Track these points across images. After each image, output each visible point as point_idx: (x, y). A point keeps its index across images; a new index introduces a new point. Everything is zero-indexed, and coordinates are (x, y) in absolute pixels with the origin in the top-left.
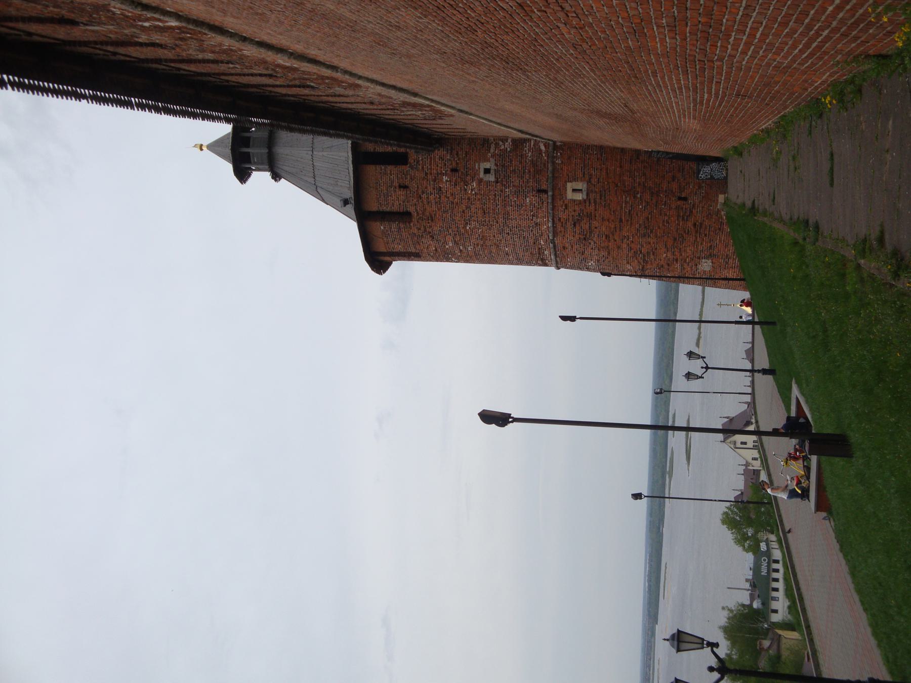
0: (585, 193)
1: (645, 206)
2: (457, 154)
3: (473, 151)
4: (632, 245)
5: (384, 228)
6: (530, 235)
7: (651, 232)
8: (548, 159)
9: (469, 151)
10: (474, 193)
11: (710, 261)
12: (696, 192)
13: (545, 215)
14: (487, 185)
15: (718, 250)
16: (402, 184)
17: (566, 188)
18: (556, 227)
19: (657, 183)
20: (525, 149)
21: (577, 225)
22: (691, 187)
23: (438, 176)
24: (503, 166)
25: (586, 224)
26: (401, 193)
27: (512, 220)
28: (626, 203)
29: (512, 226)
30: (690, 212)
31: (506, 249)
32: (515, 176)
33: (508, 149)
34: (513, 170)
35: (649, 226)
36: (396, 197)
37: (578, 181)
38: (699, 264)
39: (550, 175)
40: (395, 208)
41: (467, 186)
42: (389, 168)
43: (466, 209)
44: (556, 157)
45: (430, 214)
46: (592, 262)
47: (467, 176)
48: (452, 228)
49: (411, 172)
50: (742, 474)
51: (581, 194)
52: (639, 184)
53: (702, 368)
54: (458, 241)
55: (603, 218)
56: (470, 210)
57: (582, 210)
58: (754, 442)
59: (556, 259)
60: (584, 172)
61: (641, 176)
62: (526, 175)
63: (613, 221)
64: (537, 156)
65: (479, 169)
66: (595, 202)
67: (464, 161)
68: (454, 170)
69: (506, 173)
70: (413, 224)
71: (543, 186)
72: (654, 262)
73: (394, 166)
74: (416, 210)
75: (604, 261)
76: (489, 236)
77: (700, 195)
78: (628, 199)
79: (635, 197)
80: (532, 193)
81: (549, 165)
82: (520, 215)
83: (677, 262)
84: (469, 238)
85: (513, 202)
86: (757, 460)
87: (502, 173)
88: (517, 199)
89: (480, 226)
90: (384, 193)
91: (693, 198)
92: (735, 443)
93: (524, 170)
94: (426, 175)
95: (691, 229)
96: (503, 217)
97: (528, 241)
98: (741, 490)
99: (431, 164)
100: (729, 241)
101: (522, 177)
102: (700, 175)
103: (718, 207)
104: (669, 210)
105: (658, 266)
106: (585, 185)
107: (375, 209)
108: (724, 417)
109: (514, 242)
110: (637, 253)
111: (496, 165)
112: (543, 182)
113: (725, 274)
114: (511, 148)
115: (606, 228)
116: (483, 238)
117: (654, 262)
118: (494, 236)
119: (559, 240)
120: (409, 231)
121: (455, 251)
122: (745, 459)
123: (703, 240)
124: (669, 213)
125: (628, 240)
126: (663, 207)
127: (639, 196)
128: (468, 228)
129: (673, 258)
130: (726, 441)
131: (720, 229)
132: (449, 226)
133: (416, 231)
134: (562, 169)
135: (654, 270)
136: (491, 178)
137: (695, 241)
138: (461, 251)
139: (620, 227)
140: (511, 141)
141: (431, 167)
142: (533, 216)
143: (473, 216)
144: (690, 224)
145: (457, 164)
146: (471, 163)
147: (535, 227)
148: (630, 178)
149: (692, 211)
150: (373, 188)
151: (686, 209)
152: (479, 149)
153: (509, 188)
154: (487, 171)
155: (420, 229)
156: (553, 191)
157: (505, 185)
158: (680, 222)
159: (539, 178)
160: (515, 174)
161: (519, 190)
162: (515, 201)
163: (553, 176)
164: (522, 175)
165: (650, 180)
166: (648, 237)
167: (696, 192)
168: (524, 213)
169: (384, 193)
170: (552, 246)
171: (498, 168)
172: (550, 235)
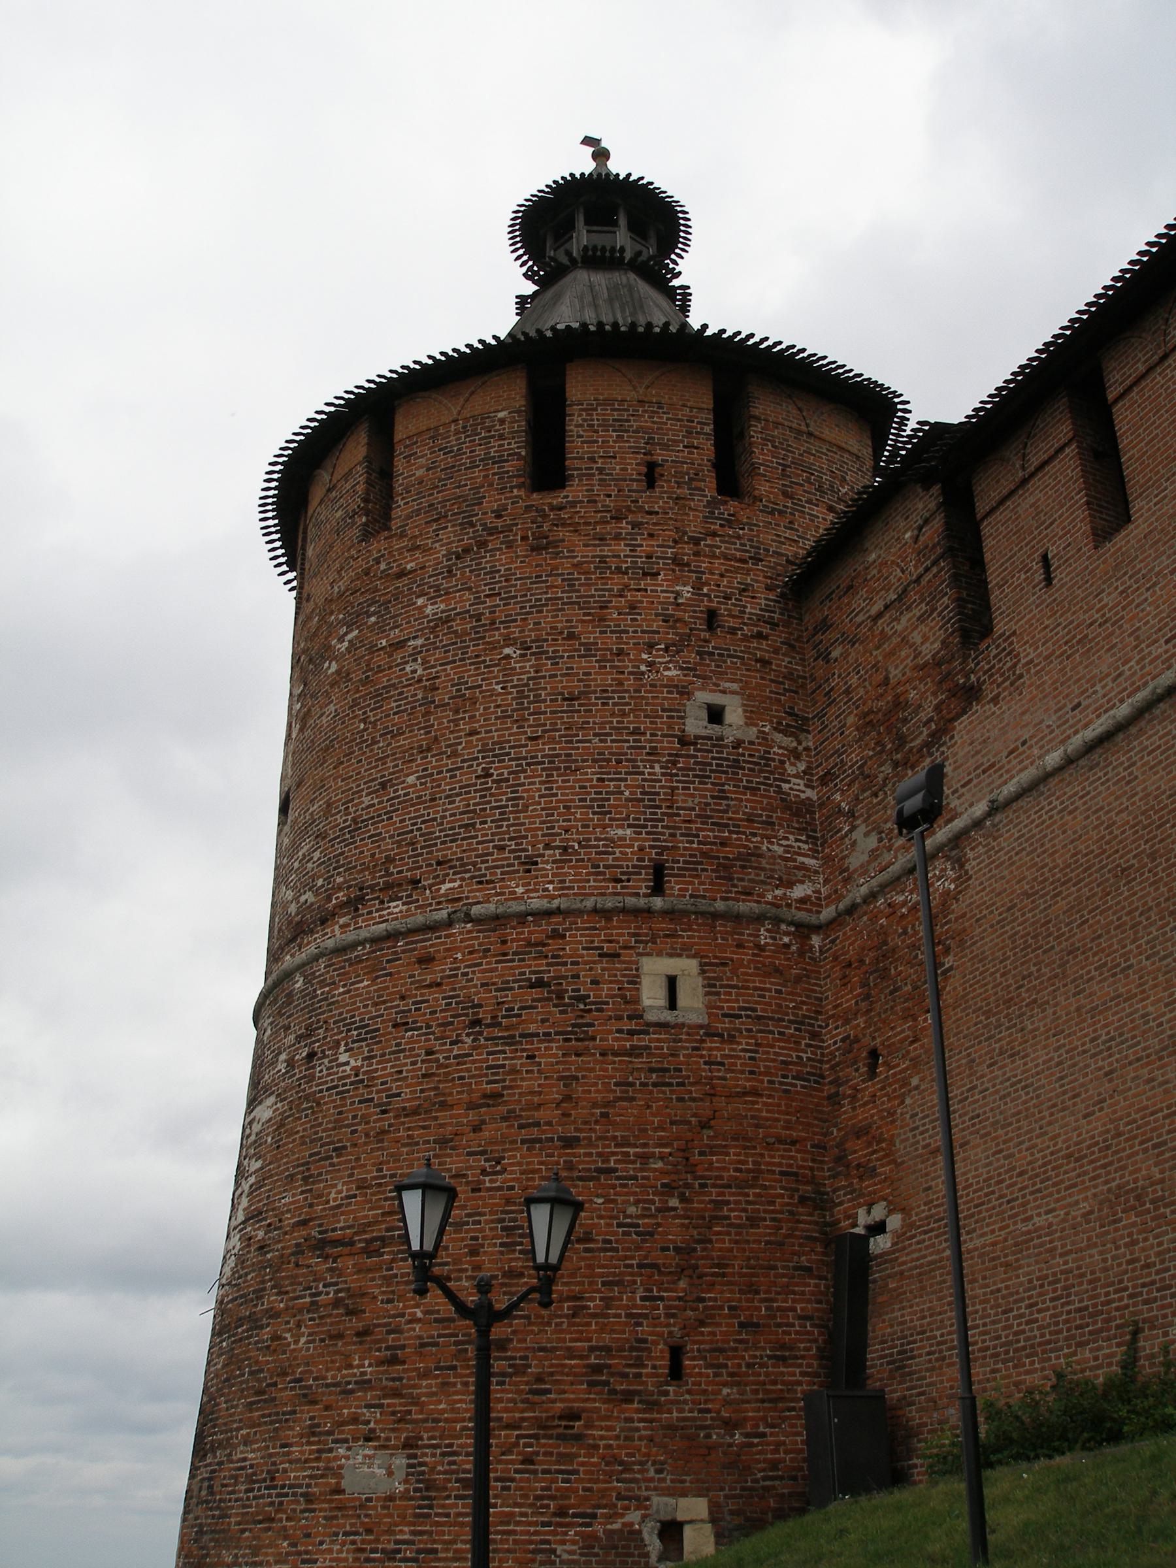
0: (667, 1016)
1: (638, 1226)
2: (760, 636)
3: (771, 681)
5: (502, 421)
8: (767, 903)
9: (771, 670)
10: (643, 668)
12: (708, 1411)
14: (671, 711)
16: (658, 470)
17: (680, 956)
18: (523, 923)
19: (726, 1266)
20: (791, 837)
21: (535, 993)
22: (725, 1391)
26: (633, 466)
28: (645, 1158)
30: (623, 1392)
32: (705, 797)
33: (785, 786)
34: (724, 791)
41: (666, 650)
42: (709, 446)
47: (698, 653)
52: (718, 1205)
55: (576, 1078)
57: (600, 1006)
59: (362, 943)
60: (740, 1016)
61: (745, 1210)
62: (712, 831)
64: (773, 870)
65: (724, 692)
66: (634, 1052)
68: (711, 617)
69: (711, 771)
71: (677, 883)
73: (712, 457)
74: (573, 504)
79: (668, 1189)
80: (651, 847)
82: (567, 808)
84: (455, 662)
87: (713, 758)
93: (727, 825)
96: (559, 755)
99: (726, 557)
101: (703, 818)
103: (656, 1500)
106: (695, 1018)
111: (738, 744)
112: (692, 883)
114: (789, 794)
116: (463, 702)
118: (473, 733)
125: (484, 1172)
131: (561, 1512)
134: (740, 945)
136: (696, 724)
139: (539, 1141)
140: (808, 799)
141: (719, 558)
142: (565, 849)
144: (576, 1395)
145: (733, 631)
146: (738, 668)
151: (639, 1375)
152: (780, 700)
153: (663, 774)
157: (674, 763)
159: (706, 870)
160: (713, 797)
161: (660, 807)
162: (622, 793)
163: (715, 916)
164: (711, 817)
165: (736, 1242)
167: (708, 1411)
172: (491, 907)
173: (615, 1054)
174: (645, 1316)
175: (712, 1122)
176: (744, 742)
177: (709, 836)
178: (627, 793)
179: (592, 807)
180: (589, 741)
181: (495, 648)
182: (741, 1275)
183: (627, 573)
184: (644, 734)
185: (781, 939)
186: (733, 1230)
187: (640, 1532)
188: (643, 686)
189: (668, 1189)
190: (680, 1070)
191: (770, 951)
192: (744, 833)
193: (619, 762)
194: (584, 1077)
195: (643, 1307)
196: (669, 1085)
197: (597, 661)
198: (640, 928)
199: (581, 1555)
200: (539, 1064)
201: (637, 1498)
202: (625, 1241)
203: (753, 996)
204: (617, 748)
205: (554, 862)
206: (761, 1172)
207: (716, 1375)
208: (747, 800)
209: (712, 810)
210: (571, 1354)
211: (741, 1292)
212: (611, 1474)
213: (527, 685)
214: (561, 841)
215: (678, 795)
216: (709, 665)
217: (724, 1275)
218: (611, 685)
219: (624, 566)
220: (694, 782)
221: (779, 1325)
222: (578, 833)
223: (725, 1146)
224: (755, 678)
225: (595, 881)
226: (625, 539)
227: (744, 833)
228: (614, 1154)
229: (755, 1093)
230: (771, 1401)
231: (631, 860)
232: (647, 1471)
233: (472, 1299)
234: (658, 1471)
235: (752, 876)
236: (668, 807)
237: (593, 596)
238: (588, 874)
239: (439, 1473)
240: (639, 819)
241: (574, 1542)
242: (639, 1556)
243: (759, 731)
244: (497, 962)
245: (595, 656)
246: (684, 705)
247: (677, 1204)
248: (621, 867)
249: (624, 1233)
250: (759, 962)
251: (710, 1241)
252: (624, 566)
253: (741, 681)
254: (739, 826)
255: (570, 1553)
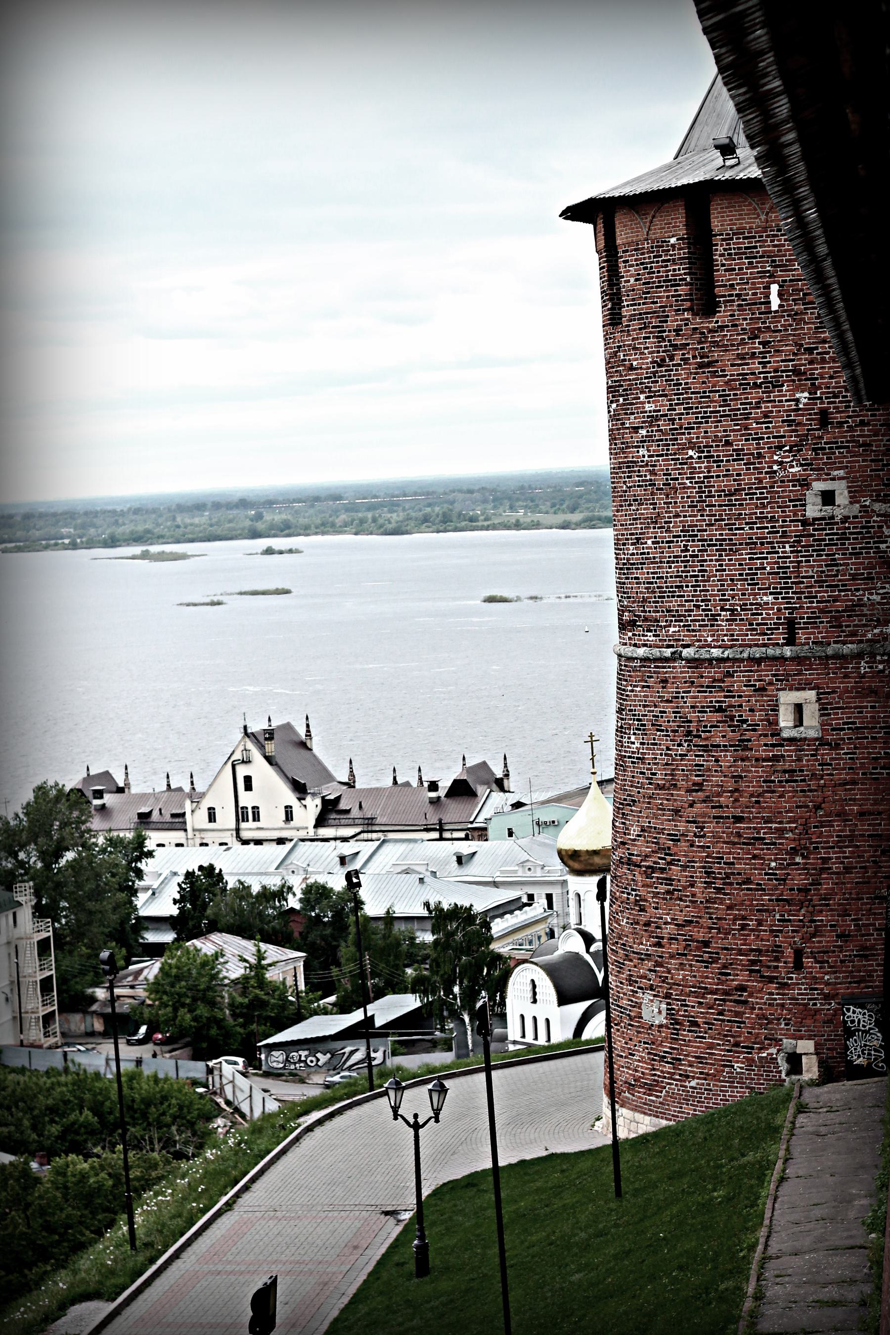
0: (794, 733)
1: (776, 874)
2: (862, 423)
3: (872, 461)
4: (683, 845)
5: (673, 246)
6: (686, 601)
7: (719, 890)
8: (868, 641)
9: (872, 451)
10: (775, 468)
11: (665, 1021)
12: (816, 989)
13: (737, 640)
15: (689, 1041)
17: (804, 689)
19: (829, 899)
21: (718, 716)
22: (827, 977)
23: (806, 380)
24: (843, 537)
25: (724, 736)
27: (717, 560)
28: (781, 831)
29: (706, 561)
31: (649, 542)
34: (835, 560)
35: (731, 884)
36: (748, 279)
37: (822, 715)
38: (655, 996)
39: (830, 651)
40: (721, 276)
41: (790, 451)
43: (734, 450)
44: (872, 661)
45: (717, 361)
46: (637, 745)
47: (814, 450)
48: (688, 414)
49: (812, 313)
50: (169, 785)
51: (791, 724)
52: (825, 860)
53: (416, 1116)
54: (659, 426)
55: (741, 777)
56: (734, 460)
58: (253, 808)
60: (844, 729)
61: (843, 863)
62: (827, 592)
63: (736, 800)
65: (833, 479)
66: (776, 758)
67: (847, 442)
68: (824, 418)
69: (826, 545)
70: (687, 319)
72: (649, 892)
74: (722, 328)
75: (642, 773)
76: (676, 503)
77: (809, 999)
78: (790, 835)
79: (794, 852)
80: (786, 608)
81: (855, 646)
83: (655, 945)
84: (667, 455)
85: (762, 564)
86: (210, 821)
87: (827, 535)
88: (769, 573)
89: (696, 483)
90: (756, 247)
91: (803, 984)
92: (246, 762)
93: (837, 586)
94: (805, 349)
95: (733, 980)
96: (725, 540)
97: (673, 597)
98: (127, 785)
100: (714, 1065)
102: (852, 1008)
103: (785, 1041)
104: (772, 931)
105: (641, 900)
106: (812, 734)
107: (716, 224)
108: (308, 726)
109: (668, 562)
110: (666, 854)
111: (845, 519)
112: (814, 633)
113: (639, 1051)
115: (718, 786)
116: (670, 489)
117: (649, 892)
118: (677, 516)
119: (682, 672)
120: (671, 306)
121: (633, 414)
122: (208, 790)
123: (709, 1008)
124: (765, 931)
125: (695, 836)
126: (777, 917)
127: (798, 859)
128: (691, 453)
129: (663, 938)
130: (247, 739)
131: (737, 1044)
132: (691, 408)
133: (672, 324)
134: (846, 676)
135: (633, 890)
137: (706, 988)
138: (636, 429)
139: (722, 817)
142: (732, 611)
143: (718, 466)
144: (742, 978)
145: (841, 424)
146: (845, 457)
147: (707, 615)
148: (837, 836)
149: (772, 982)
150: (767, 221)
151: (777, 967)
153: (792, 552)
154: (828, 498)
155: (678, 335)
156: (794, 659)
157: (799, 542)
158: (746, 955)
159: (823, 622)
160: (826, 566)
161: (790, 578)
162: (765, 568)
163: (828, 657)
164: (826, 581)
165: (836, 884)
166: (705, 882)
167: (816, 989)
168: (738, 590)
169: (756, 247)
170: (666, 655)
171: (837, 523)
173: (764, 760)
174: (781, 931)
175: (823, 805)
176: (849, 517)
177: (824, 597)
178: (768, 569)
179: (746, 580)
180: (743, 529)
181: (683, 449)
182: (839, 905)
183: (761, 388)
184: (778, 521)
185: (877, 667)
186: (834, 876)
187: (776, 1059)
188: (776, 482)
189: (794, 852)
190: (803, 771)
191: (868, 677)
192: (850, 590)
193: (762, 544)
194: (745, 776)
195: (778, 926)
196: (796, 781)
197: (745, 464)
198: (778, 670)
199: (747, 1070)
200: (721, 766)
201: (775, 1040)
202: (769, 885)
203: (853, 713)
204: (761, 533)
205: (727, 620)
206: (856, 836)
207: (821, 968)
208: (853, 564)
209: (826, 576)
210: (740, 952)
211: (839, 915)
212: (761, 1025)
213: (703, 482)
214: (730, 605)
215: (803, 567)
216: (822, 459)
217: (828, 905)
218: (754, 484)
219: (759, 381)
220: (812, 556)
221: (863, 935)
222: (740, 600)
223: (830, 821)
224: (858, 461)
225: (751, 635)
226: (758, 357)
227: (850, 590)
228: (762, 828)
229: (854, 782)
230: (855, 982)
231: (772, 619)
232: (781, 1024)
233: (412, 1121)
234: (786, 1025)
235: (856, 622)
236: (796, 577)
237: (739, 409)
238: (747, 630)
239: (681, 1016)
240: (776, 588)
241: (743, 1063)
242: (776, 1072)
243: (861, 506)
244: (699, 692)
245: (743, 460)
246: (805, 495)
247: (801, 861)
248: (766, 624)
249: (769, 879)
250: (860, 687)
251: (820, 884)
252: (759, 381)
253: (847, 467)
254: (845, 585)
255: (741, 1068)
